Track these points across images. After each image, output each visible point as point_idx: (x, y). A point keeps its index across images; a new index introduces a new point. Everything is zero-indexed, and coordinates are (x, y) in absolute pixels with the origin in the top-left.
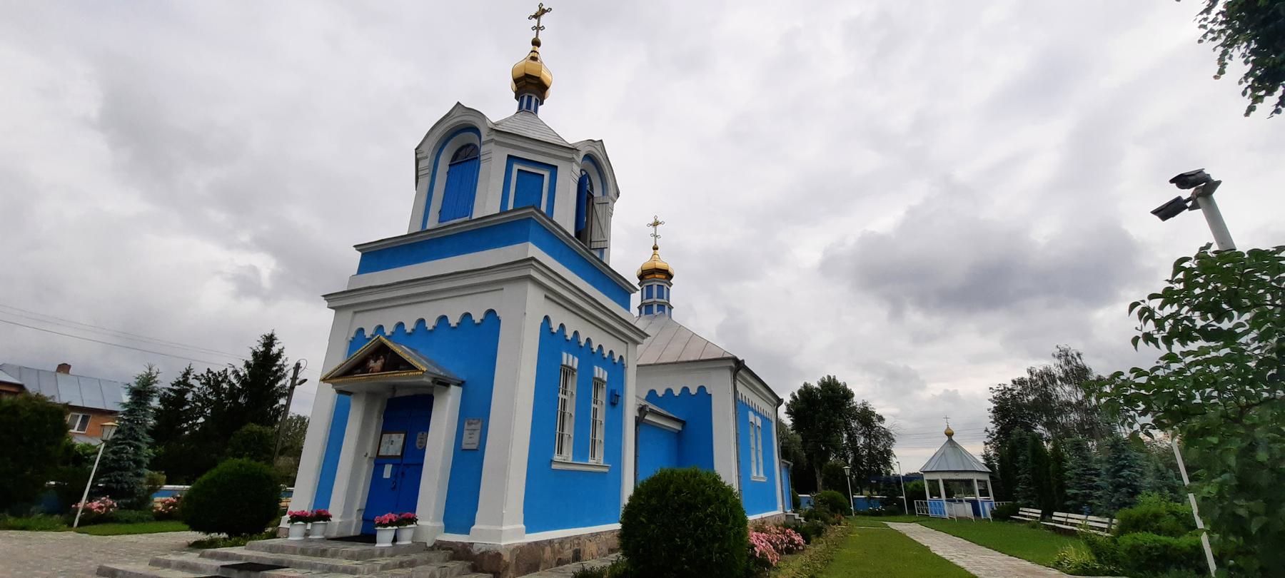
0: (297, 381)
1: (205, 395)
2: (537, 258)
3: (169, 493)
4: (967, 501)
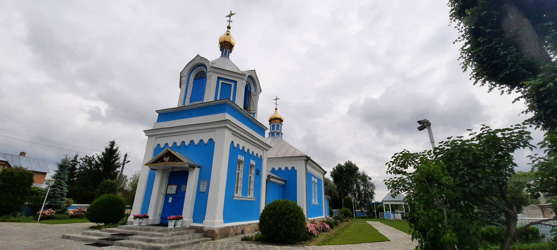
0: (126, 162)
1: (85, 167)
2: (229, 119)
3: (74, 208)
4: (400, 213)
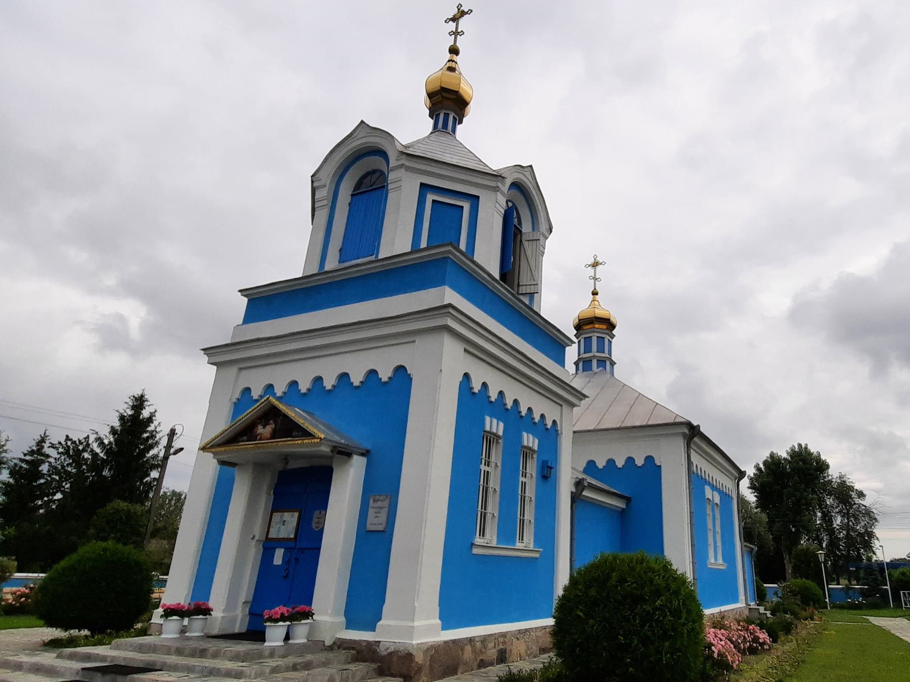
0: (172, 451)
1: (63, 467)
